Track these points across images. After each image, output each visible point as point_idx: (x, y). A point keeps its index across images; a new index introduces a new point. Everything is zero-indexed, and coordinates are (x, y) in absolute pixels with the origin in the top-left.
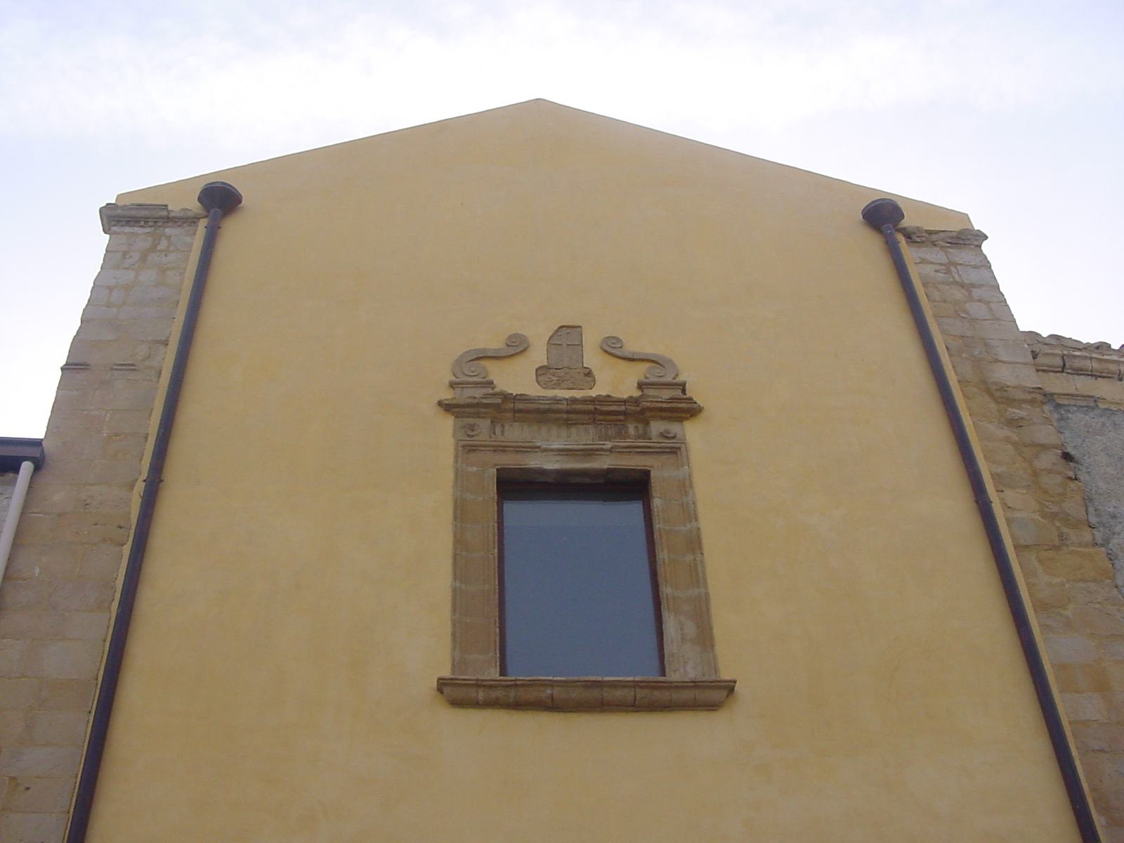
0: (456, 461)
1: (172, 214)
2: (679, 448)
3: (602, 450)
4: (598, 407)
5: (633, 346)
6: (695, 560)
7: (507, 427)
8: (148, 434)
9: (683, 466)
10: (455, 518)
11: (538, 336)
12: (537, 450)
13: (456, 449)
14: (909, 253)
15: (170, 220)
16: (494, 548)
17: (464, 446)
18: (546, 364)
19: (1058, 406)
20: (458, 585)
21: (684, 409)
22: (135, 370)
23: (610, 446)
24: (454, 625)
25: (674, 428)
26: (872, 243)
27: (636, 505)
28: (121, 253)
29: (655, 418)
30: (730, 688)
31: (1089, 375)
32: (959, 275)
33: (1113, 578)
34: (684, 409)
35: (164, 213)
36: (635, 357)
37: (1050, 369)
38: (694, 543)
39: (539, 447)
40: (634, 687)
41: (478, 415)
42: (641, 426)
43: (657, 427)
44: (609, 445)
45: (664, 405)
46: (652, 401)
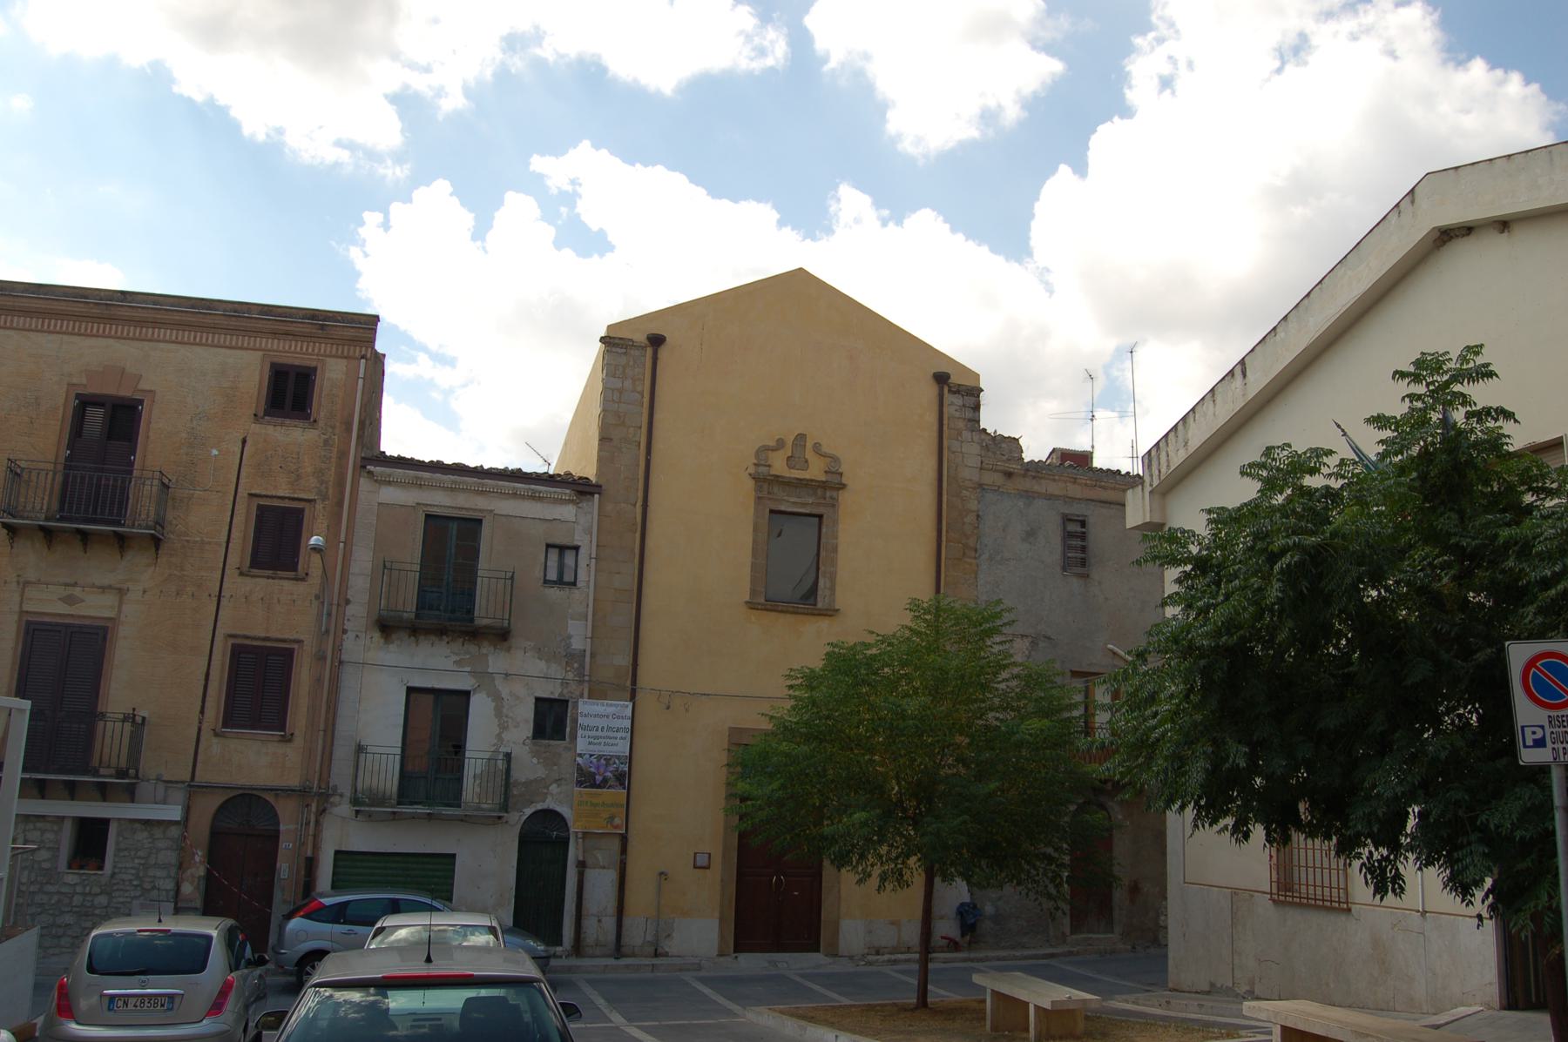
5: (825, 449)
11: (790, 440)
14: (948, 398)
19: (984, 489)
21: (843, 486)
25: (834, 494)
27: (257, 378)
28: (1030, 639)
30: (838, 610)
38: (835, 549)
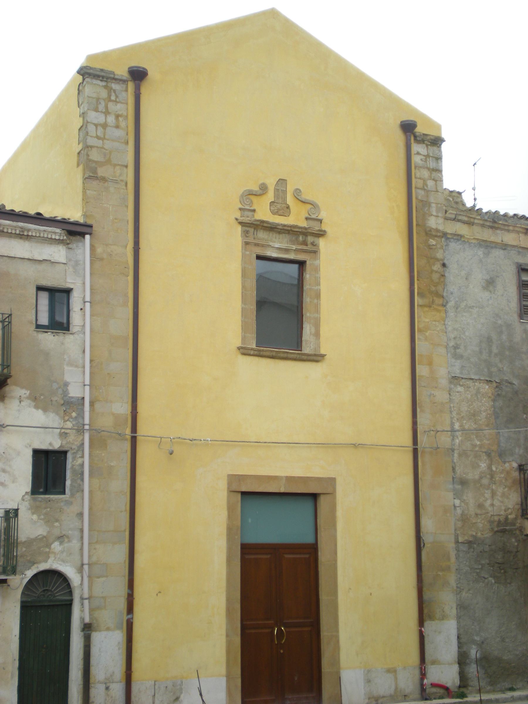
0: (242, 250)
1: (116, 77)
2: (317, 251)
3: (292, 250)
4: (292, 229)
6: (317, 302)
7: (258, 231)
8: (128, 220)
9: (317, 260)
10: (242, 276)
11: (271, 183)
12: (270, 246)
13: (242, 243)
15: (115, 80)
16: (255, 291)
17: (245, 242)
18: (273, 200)
20: (243, 306)
22: (117, 183)
23: (294, 248)
24: (242, 323)
25: (316, 240)
26: (399, 137)
29: (310, 235)
30: (323, 356)
31: (463, 222)
32: (430, 163)
33: (444, 321)
34: (321, 234)
35: (112, 76)
36: (306, 202)
37: (449, 219)
38: (318, 296)
39: (271, 245)
40: (297, 354)
41: (250, 227)
42: (304, 237)
43: (310, 239)
44: (294, 247)
45: (315, 232)
46: (311, 230)
